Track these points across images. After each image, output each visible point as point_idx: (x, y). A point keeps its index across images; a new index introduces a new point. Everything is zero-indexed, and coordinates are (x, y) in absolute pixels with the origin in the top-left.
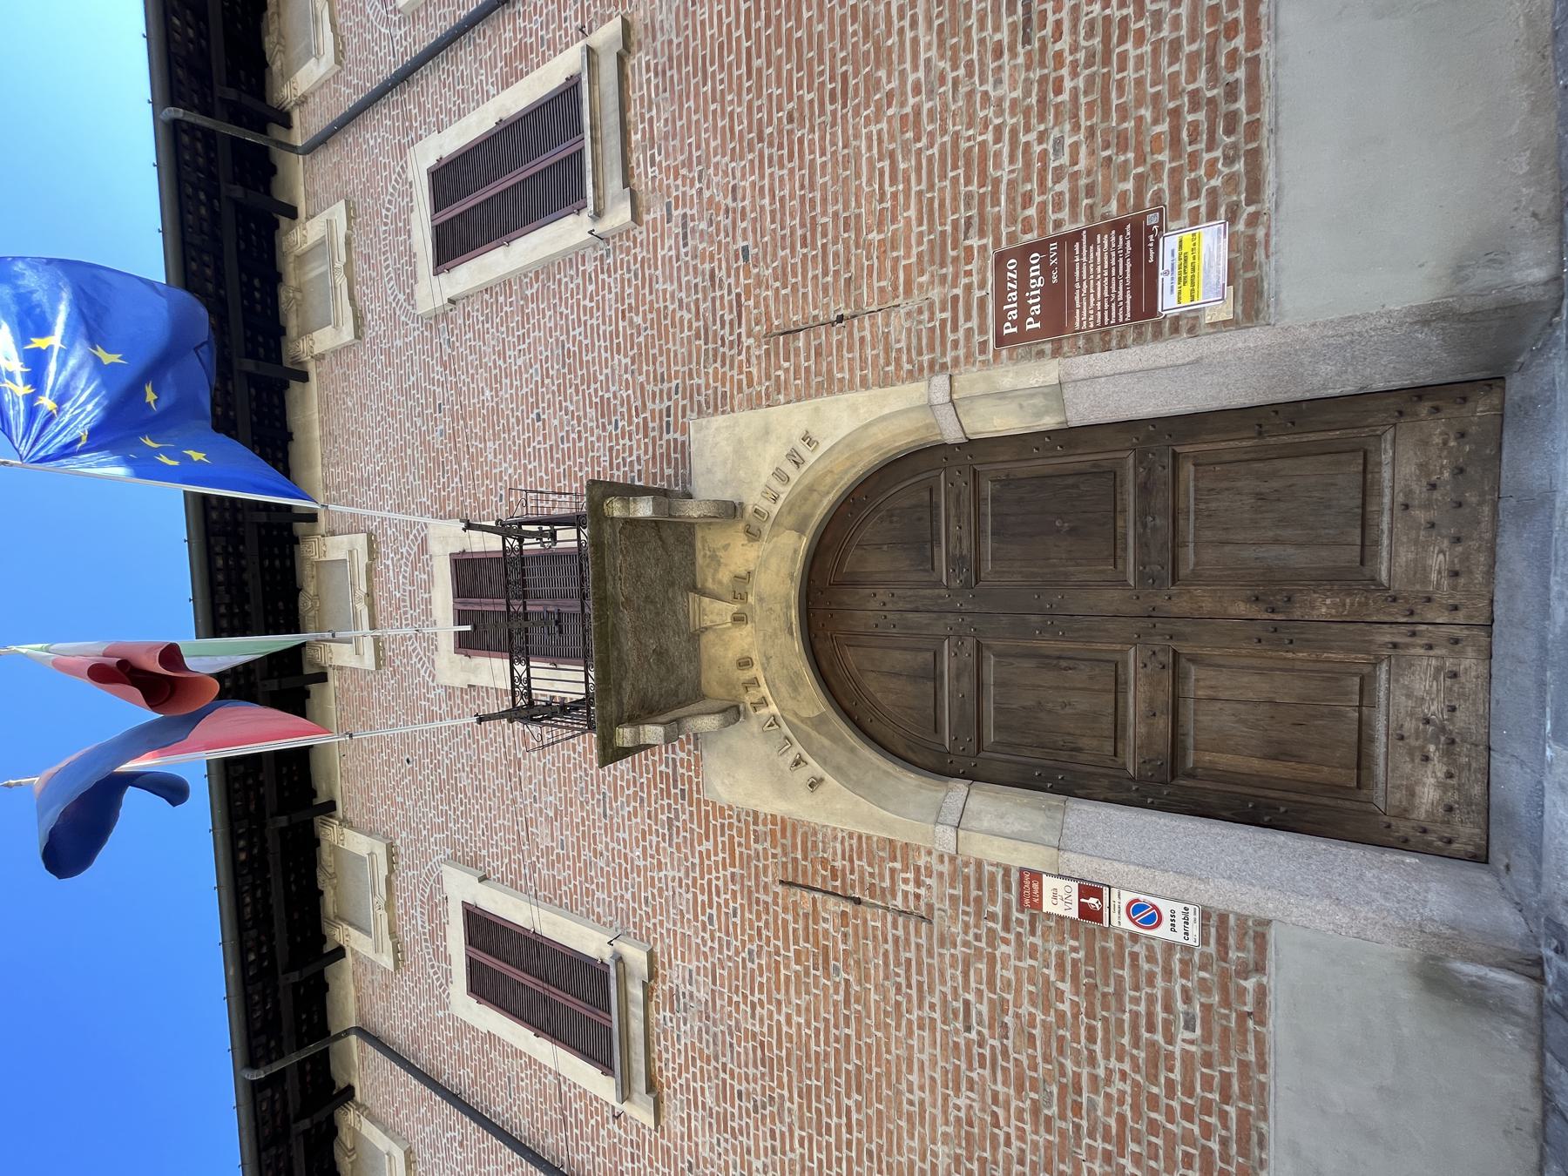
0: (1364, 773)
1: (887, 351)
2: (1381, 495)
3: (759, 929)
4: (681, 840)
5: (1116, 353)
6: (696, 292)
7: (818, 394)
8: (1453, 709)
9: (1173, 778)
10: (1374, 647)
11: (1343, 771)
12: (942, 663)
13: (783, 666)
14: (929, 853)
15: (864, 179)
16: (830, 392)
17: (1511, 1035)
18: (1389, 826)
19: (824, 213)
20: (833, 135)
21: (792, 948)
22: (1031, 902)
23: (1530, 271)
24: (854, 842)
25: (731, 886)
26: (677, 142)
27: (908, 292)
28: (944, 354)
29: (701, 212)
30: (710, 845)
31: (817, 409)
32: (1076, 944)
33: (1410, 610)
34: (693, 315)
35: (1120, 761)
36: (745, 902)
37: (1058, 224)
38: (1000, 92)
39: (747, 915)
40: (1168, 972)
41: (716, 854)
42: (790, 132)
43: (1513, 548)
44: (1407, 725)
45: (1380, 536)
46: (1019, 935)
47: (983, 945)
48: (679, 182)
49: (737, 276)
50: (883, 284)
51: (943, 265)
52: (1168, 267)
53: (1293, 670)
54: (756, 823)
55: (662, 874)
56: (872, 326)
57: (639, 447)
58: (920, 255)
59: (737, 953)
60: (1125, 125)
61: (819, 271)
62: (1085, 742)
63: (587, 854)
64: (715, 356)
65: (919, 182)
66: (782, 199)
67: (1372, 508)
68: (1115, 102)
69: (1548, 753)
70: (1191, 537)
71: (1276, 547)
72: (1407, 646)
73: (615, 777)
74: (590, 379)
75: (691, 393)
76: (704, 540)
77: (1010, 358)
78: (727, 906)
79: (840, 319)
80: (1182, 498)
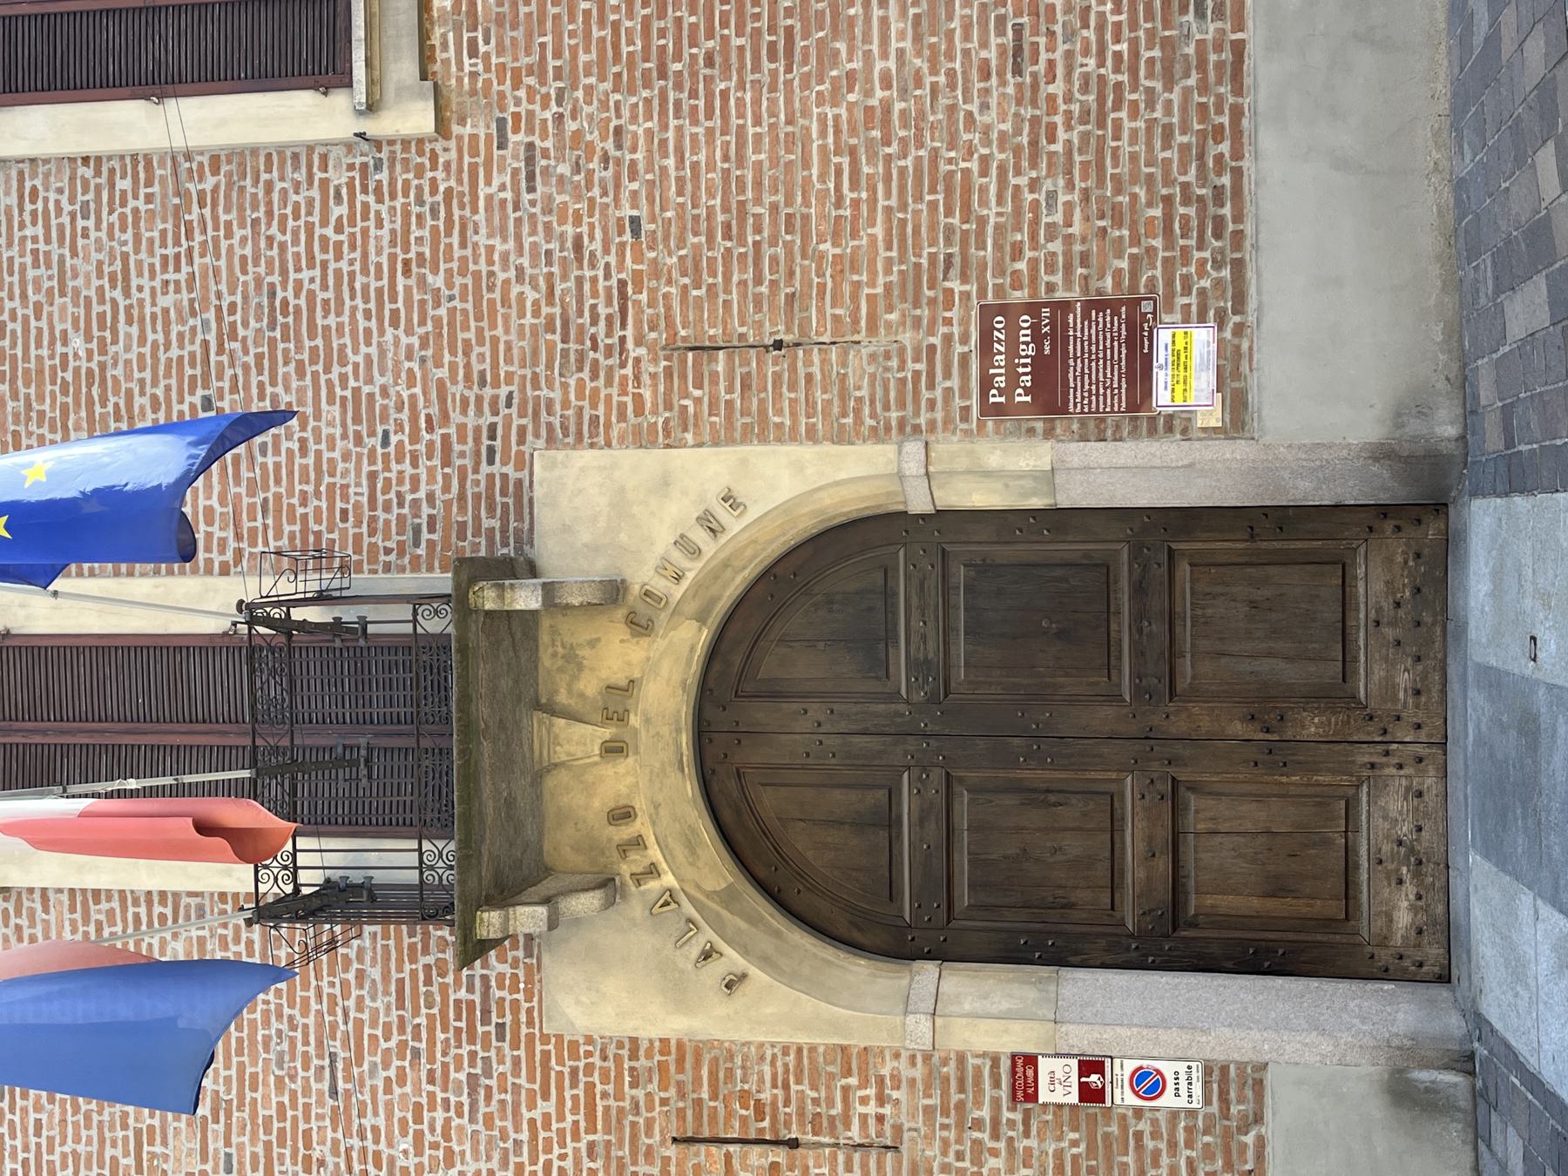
0: (1351, 902)
1: (844, 396)
2: (1358, 610)
5: (1111, 445)
7: (746, 439)
8: (1420, 829)
9: (1174, 930)
11: (1334, 903)
12: (900, 804)
14: (897, 1056)
15: (815, 171)
16: (763, 439)
17: (1454, 1133)
18: (1372, 957)
19: (758, 201)
20: (773, 102)
24: (791, 1058)
26: (519, 34)
27: (872, 328)
28: (917, 413)
30: (550, 1107)
31: (744, 462)
32: (1074, 1136)
34: (540, 296)
35: (1117, 914)
38: (986, 119)
40: (1172, 1145)
42: (709, 80)
48: (522, 93)
51: (917, 304)
52: (1162, 361)
54: (634, 1056)
56: (823, 361)
60: (1120, 198)
61: (749, 275)
65: (888, 195)
66: (695, 166)
67: (1350, 623)
68: (1110, 171)
72: (1382, 766)
76: (554, 631)
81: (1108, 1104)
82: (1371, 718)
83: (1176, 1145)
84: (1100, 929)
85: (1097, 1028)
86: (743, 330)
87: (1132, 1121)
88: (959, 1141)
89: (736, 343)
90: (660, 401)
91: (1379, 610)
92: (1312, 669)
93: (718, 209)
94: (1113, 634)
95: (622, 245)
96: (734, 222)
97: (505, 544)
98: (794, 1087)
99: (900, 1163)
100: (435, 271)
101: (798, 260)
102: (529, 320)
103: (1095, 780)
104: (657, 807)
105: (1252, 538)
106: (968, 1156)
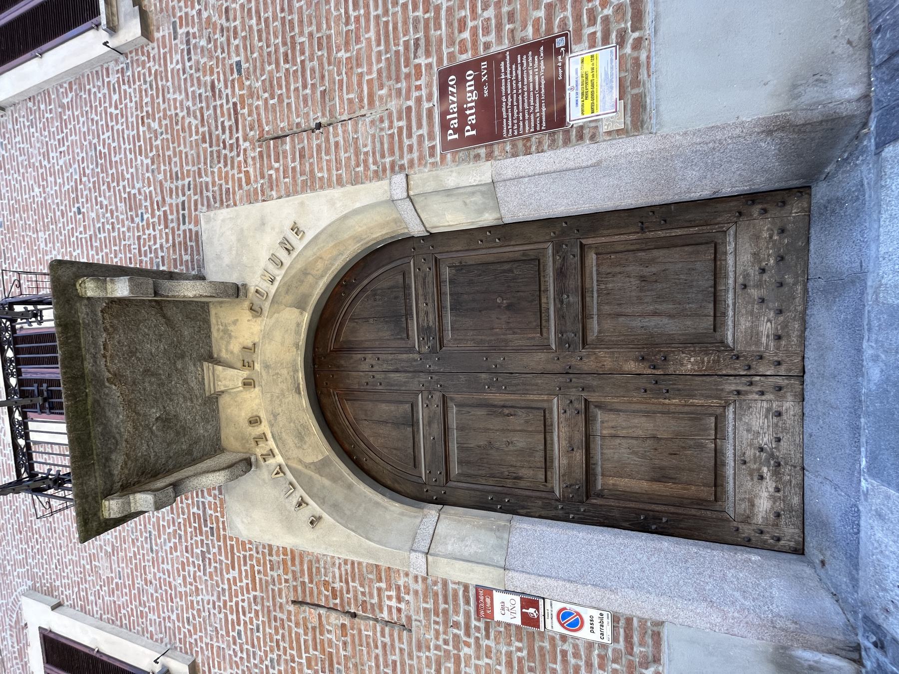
0: (719, 489)
1: (357, 153)
2: (726, 277)
3: (277, 641)
4: (212, 570)
5: (535, 156)
6: (201, 102)
7: (303, 191)
8: (778, 440)
9: (587, 498)
10: (724, 394)
11: (705, 489)
12: (418, 412)
13: (291, 420)
16: (313, 189)
18: (737, 529)
19: (301, 33)
21: (304, 655)
22: (486, 614)
23: (846, 89)
24: (349, 567)
25: (254, 607)
27: (371, 103)
28: (401, 157)
29: (200, 30)
30: (236, 573)
31: (302, 204)
32: (520, 645)
33: (747, 364)
34: (198, 122)
36: (266, 619)
37: (487, 46)
39: (268, 630)
41: (241, 581)
43: (824, 321)
44: (748, 453)
45: (726, 309)
46: (477, 638)
47: (450, 648)
49: (233, 87)
50: (351, 96)
51: (398, 80)
52: (573, 83)
53: (668, 413)
54: (270, 554)
55: (199, 598)
56: (344, 132)
57: (161, 237)
58: (379, 72)
59: (262, 662)
61: (300, 84)
62: (523, 472)
63: (139, 582)
64: (219, 157)
66: (267, 20)
69: (863, 484)
70: (595, 310)
71: (656, 318)
72: (746, 393)
73: (158, 518)
74: (118, 178)
75: (200, 189)
77: (454, 161)
78: (252, 623)
79: (319, 126)
80: (588, 280)
81: (542, 629)
82: (738, 358)
83: (591, 665)
84: (538, 494)
85: (533, 577)
86: (298, 120)
87: (559, 643)
88: (445, 633)
89: (295, 129)
90: (258, 173)
91: (746, 276)
92: (689, 323)
93: (280, 44)
94: (543, 305)
95: (233, 80)
96: (289, 51)
97: (193, 269)
98: (351, 584)
99: (411, 638)
100: (154, 120)
101: (326, 67)
102: (194, 137)
103: (533, 401)
104: (275, 416)
105: (642, 230)
106: (451, 643)
